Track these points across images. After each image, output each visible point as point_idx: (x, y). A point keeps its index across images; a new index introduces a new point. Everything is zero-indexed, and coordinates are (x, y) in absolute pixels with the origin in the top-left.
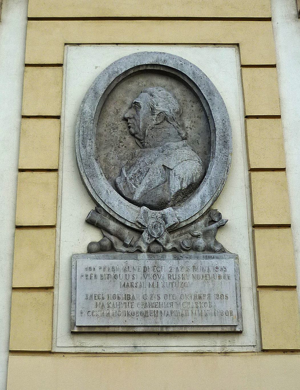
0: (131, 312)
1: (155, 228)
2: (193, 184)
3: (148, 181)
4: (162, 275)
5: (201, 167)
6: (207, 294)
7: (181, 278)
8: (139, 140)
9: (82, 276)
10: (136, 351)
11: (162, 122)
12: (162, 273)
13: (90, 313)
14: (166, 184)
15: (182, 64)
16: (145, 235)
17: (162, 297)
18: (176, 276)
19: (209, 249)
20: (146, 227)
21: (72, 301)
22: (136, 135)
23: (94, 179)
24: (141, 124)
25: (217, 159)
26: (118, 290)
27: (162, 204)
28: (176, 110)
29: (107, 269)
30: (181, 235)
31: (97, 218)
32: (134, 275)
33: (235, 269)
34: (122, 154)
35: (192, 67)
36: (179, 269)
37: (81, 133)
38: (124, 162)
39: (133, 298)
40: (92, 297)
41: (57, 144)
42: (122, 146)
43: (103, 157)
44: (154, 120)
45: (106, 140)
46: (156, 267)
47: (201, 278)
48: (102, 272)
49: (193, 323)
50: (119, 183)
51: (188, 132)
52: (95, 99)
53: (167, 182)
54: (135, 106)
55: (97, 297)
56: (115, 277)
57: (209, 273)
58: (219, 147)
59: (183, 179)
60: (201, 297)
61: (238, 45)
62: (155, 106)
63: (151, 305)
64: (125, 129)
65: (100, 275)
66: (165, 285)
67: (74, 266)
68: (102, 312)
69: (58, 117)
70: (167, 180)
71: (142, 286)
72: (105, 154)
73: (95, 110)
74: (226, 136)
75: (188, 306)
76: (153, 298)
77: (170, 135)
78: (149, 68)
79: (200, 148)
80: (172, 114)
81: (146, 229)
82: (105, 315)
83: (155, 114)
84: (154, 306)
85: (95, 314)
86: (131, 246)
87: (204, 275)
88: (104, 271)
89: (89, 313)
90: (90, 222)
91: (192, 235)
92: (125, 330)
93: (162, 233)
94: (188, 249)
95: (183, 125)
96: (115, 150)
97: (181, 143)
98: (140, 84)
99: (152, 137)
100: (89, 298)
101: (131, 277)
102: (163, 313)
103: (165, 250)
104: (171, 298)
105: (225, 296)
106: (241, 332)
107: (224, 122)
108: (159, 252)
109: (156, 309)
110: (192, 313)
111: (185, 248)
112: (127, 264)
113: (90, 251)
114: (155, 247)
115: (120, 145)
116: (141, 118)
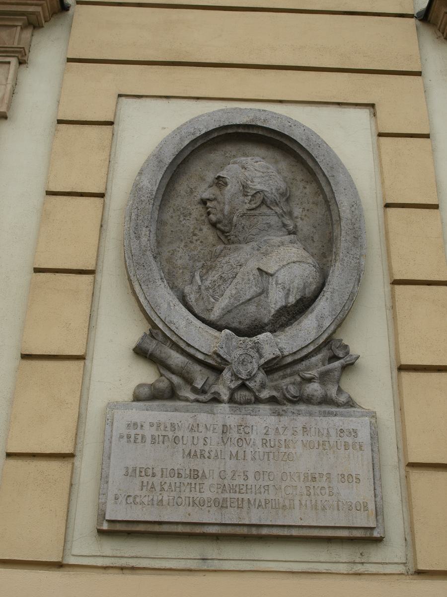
0: (198, 499)
1: (242, 363)
2: (304, 300)
3: (234, 292)
4: (252, 440)
5: (317, 274)
6: (325, 474)
7: (284, 446)
8: (223, 232)
9: (121, 437)
10: (205, 568)
11: (259, 206)
12: (252, 437)
13: (131, 500)
14: (262, 297)
15: (291, 126)
16: (226, 374)
17: (251, 475)
18: (275, 442)
19: (326, 401)
20: (228, 362)
21: (103, 478)
22: (219, 226)
23: (149, 286)
24: (227, 208)
25: (343, 263)
26: (178, 462)
27: (255, 328)
28: (281, 190)
29: (162, 427)
30: (284, 377)
31: (151, 346)
32: (206, 439)
33: (371, 434)
34: (196, 253)
35: (306, 131)
36: (281, 430)
37: (133, 217)
38: (199, 264)
39: (204, 475)
40: (135, 473)
41: (98, 237)
42: (196, 241)
43: (166, 255)
44: (246, 203)
45: (172, 231)
46: (243, 427)
47: (316, 445)
48: (153, 431)
49: (302, 521)
50: (189, 295)
51: (298, 224)
52: (158, 169)
53: (265, 294)
54: (220, 182)
55: (143, 474)
56: (176, 440)
57: (328, 438)
58: (346, 245)
59: (289, 290)
60: (315, 478)
61: (373, 106)
62: (249, 182)
63: (233, 489)
64: (202, 215)
65: (150, 436)
66: (257, 457)
67: (109, 421)
68: (151, 497)
69: (102, 195)
70: (264, 292)
71: (219, 456)
72: (169, 252)
73: (158, 184)
74: (357, 229)
75: (294, 493)
76: (236, 477)
77: (270, 226)
78: (240, 130)
79: (316, 247)
80: (275, 196)
81: (228, 365)
82: (155, 503)
83: (249, 194)
84: (238, 490)
85: (138, 500)
86: (203, 391)
87: (321, 443)
88: (157, 430)
89: (128, 499)
90: (140, 352)
91: (301, 377)
92: (188, 529)
93: (254, 373)
94: (295, 399)
95: (290, 214)
96: (186, 246)
97: (287, 238)
98: (227, 155)
99: (243, 228)
100: (131, 473)
101: (202, 441)
102: (252, 502)
103: (258, 401)
104: (266, 477)
105: (354, 478)
106: (379, 540)
107: (353, 208)
108: (248, 402)
109: (240, 496)
110: (301, 504)
111: (290, 398)
112: (196, 419)
113: (137, 398)
114: (243, 395)
115: (192, 239)
116: (226, 199)
